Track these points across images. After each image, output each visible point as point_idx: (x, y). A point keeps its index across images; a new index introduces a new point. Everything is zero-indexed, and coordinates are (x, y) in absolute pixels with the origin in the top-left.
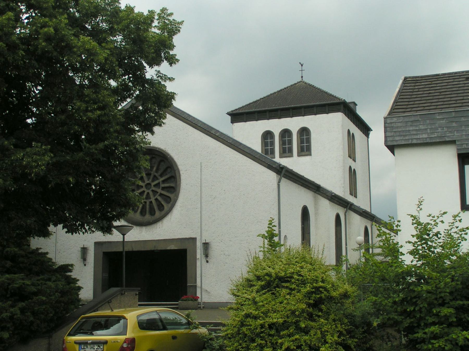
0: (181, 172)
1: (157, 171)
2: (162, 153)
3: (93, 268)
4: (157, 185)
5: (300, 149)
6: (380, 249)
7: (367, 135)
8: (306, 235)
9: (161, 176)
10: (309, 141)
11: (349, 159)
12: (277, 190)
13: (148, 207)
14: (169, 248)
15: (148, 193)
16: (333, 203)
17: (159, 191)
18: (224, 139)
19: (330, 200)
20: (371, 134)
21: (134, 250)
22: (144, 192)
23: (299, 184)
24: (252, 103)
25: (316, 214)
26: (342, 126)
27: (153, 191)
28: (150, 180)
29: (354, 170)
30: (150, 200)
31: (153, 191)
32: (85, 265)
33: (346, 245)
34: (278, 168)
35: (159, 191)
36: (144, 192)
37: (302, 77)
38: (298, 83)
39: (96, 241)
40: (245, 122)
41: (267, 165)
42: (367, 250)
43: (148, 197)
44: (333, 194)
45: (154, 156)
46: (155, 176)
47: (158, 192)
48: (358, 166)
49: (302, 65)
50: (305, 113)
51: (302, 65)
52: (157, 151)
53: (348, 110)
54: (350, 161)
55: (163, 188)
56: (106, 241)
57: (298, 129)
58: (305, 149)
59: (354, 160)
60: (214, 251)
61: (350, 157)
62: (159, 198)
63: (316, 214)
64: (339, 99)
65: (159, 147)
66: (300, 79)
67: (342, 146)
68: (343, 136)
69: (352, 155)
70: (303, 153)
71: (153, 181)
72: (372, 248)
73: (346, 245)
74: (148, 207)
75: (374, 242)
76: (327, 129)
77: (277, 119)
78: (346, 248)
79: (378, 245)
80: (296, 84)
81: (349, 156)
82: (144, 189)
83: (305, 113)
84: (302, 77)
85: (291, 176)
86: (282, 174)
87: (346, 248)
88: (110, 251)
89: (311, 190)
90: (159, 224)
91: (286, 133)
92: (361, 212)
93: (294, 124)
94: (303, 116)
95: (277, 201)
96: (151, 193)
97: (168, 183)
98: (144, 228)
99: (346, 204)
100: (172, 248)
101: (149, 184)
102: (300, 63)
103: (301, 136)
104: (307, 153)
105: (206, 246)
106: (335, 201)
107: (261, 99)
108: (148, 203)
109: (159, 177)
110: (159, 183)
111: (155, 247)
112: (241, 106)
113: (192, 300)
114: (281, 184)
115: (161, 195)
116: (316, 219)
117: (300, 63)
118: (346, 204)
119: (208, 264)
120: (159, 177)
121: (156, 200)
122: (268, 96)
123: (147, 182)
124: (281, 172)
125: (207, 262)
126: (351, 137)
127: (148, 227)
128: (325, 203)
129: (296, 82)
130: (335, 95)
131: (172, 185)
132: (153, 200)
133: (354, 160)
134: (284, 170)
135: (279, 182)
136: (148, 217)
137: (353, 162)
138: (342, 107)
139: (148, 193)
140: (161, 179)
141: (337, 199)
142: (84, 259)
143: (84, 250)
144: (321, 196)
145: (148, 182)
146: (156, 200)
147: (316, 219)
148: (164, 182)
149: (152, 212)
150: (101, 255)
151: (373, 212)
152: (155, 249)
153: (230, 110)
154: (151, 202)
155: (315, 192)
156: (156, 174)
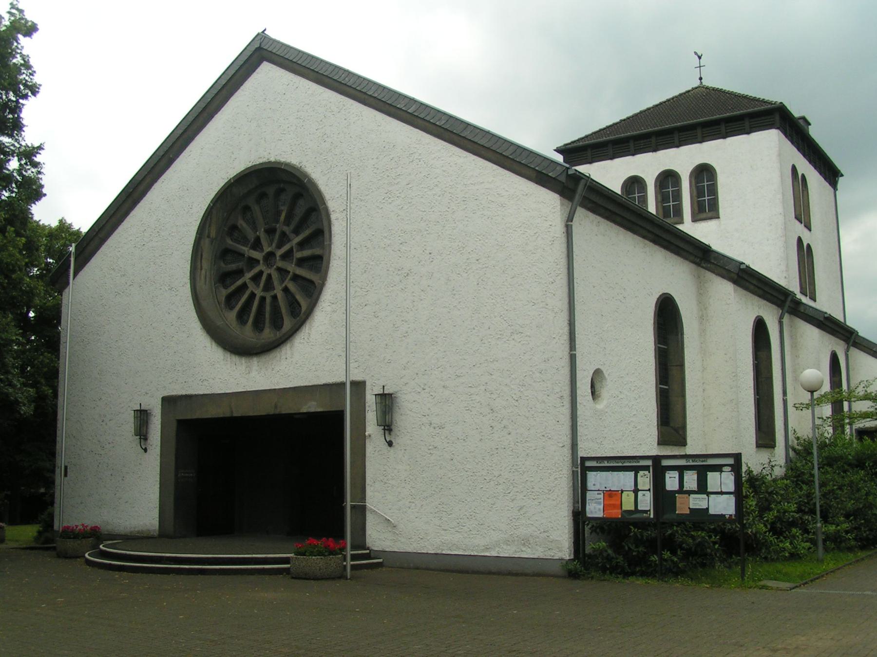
0: (333, 217)
1: (287, 222)
2: (299, 180)
3: (159, 458)
4: (287, 256)
5: (696, 208)
6: (869, 403)
7: (834, 184)
8: (674, 372)
9: (296, 232)
10: (713, 190)
11: (797, 222)
12: (564, 240)
13: (268, 308)
14: (304, 410)
15: (269, 276)
16: (744, 292)
17: (292, 268)
18: (427, 118)
19: (735, 282)
20: (841, 181)
21: (235, 415)
22: (261, 273)
23: (644, 237)
24: (604, 129)
25: (703, 318)
26: (779, 155)
27: (280, 270)
28: (274, 245)
29: (809, 246)
30: (272, 293)
31: (280, 270)
32: (145, 450)
33: (785, 393)
34: (563, 179)
35: (292, 268)
36: (261, 273)
37: (701, 79)
38: (693, 89)
39: (166, 393)
40: (590, 163)
41: (534, 175)
42: (837, 406)
43: (269, 286)
44: (742, 267)
45: (282, 186)
46: (284, 234)
47: (289, 272)
48: (815, 239)
49: (700, 58)
50: (703, 137)
51: (700, 58)
52: (284, 170)
53: (796, 130)
54: (799, 229)
55: (301, 262)
56: (184, 393)
57: (691, 168)
58: (707, 206)
59: (808, 227)
60: (407, 416)
61: (798, 218)
62: (292, 287)
63: (703, 318)
64: (770, 103)
65: (288, 161)
66: (697, 83)
67: (780, 196)
68: (782, 176)
69: (802, 215)
70: (704, 215)
71: (279, 246)
72: (850, 402)
73: (785, 393)
74: (268, 308)
75: (852, 385)
76: (751, 165)
77: (651, 154)
78: (785, 402)
79: (861, 394)
80: (689, 91)
81: (796, 218)
82: (261, 267)
83: (703, 137)
84: (701, 79)
85: (611, 207)
86: (577, 197)
87: (785, 402)
88: (189, 417)
89: (686, 258)
90: (285, 350)
91: (668, 178)
92: (822, 319)
93: (682, 159)
94: (701, 142)
95: (564, 271)
96: (275, 276)
97: (312, 248)
98: (255, 361)
99: (783, 298)
100: (312, 410)
101: (271, 255)
102: (696, 53)
103: (697, 183)
104: (710, 214)
105: (387, 401)
106: (752, 287)
107: (621, 121)
108: (268, 300)
109: (292, 236)
110: (291, 251)
111: (276, 407)
112: (583, 135)
113: (320, 554)
114: (575, 224)
115: (296, 278)
116: (703, 332)
117: (696, 53)
118: (783, 298)
119: (392, 450)
120: (292, 236)
121: (286, 290)
122: (636, 115)
123: (267, 249)
124: (574, 191)
125: (390, 444)
126: (799, 183)
127: (265, 358)
128: (723, 290)
129: (690, 88)
130: (762, 98)
131: (317, 251)
132: (278, 292)
133: (808, 227)
134: (582, 183)
135: (570, 218)
136: (268, 334)
137: (806, 230)
138: (777, 117)
139: (269, 276)
140: (297, 239)
141: (755, 282)
142: (142, 432)
143: (142, 417)
144: (713, 272)
145: (269, 249)
146: (286, 290)
147: (703, 332)
148: (302, 245)
149: (277, 323)
150: (174, 426)
151: (849, 323)
152: (277, 412)
153: (560, 144)
154: (275, 297)
155: (698, 264)
156: (286, 229)
